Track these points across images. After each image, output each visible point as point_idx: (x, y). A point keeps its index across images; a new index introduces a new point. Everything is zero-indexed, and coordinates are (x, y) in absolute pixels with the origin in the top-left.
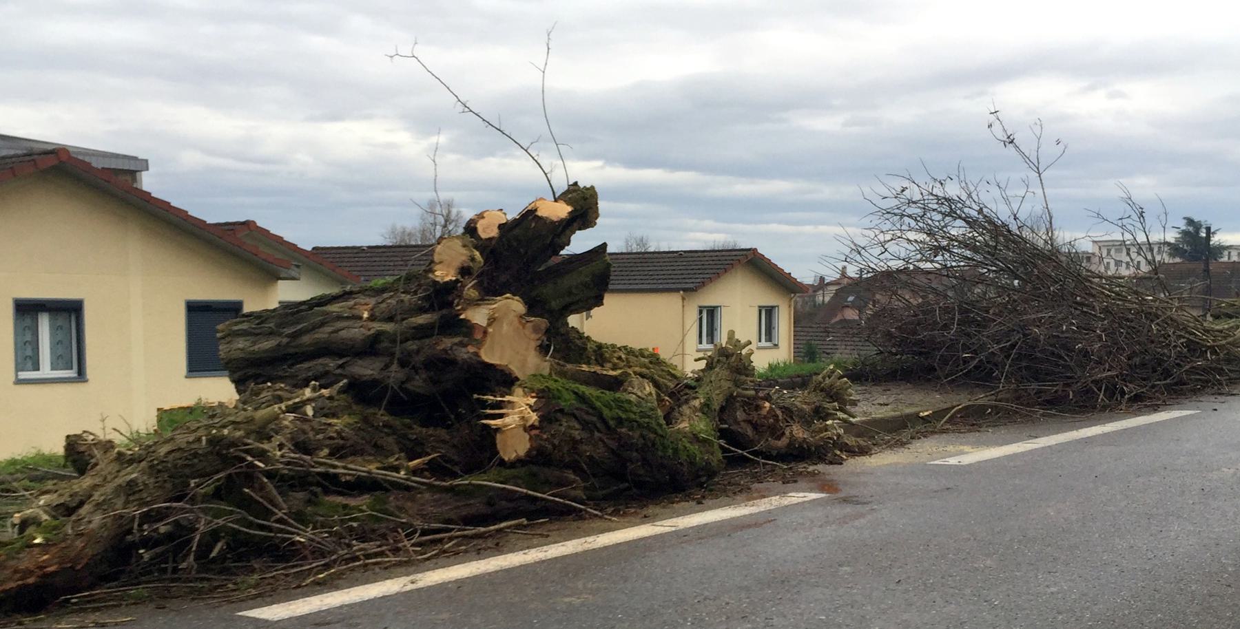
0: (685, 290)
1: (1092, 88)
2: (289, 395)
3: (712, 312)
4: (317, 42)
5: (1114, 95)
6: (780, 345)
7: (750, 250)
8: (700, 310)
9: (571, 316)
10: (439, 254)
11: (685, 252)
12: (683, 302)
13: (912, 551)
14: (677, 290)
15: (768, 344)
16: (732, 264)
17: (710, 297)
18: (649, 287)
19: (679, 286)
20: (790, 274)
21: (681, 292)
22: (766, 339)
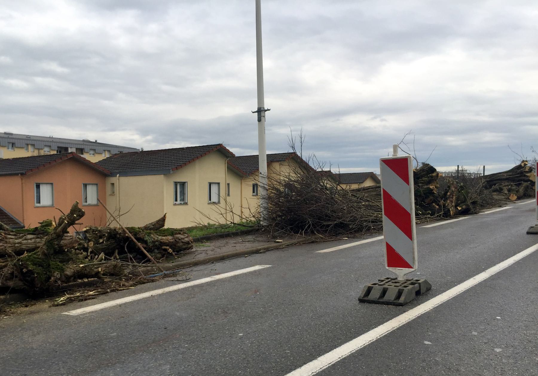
0: (359, 183)
1: (375, 118)
2: (156, 263)
3: (183, 184)
4: (106, 103)
5: (382, 120)
6: (188, 203)
7: (372, 172)
8: (210, 185)
9: (79, 206)
10: (117, 179)
11: (352, 173)
12: (22, 181)
13: (384, 339)
14: (357, 183)
15: (182, 202)
16: (197, 157)
17: (180, 178)
18: (354, 182)
19: (358, 182)
20: (96, 141)
21: (358, 183)
22: (37, 202)
